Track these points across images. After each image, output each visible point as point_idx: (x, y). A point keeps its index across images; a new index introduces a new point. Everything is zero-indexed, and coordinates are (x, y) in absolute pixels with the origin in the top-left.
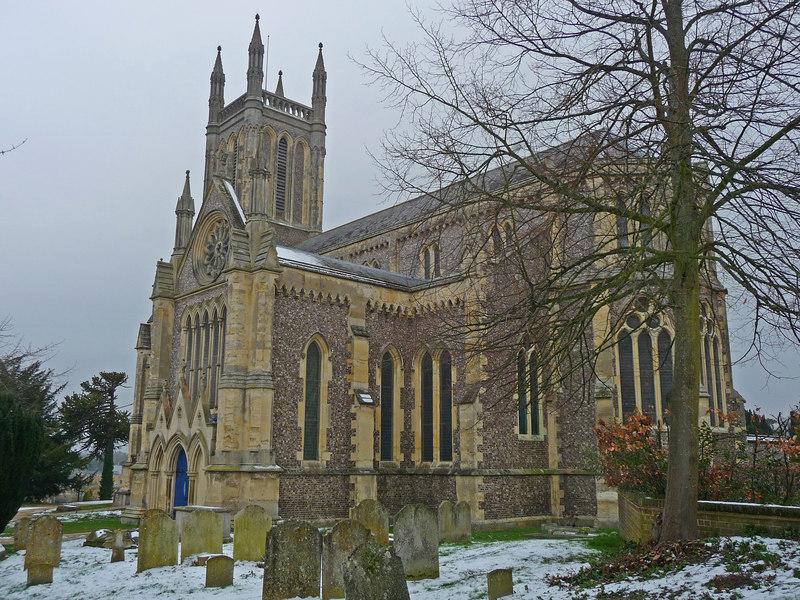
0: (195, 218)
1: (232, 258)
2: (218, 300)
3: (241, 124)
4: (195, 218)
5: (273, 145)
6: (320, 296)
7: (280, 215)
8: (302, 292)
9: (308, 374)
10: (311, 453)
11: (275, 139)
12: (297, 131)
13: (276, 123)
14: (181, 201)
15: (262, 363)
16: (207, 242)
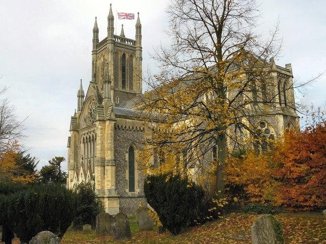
0: (85, 98)
1: (97, 116)
2: (94, 132)
3: (106, 50)
4: (85, 98)
5: (119, 57)
6: (133, 128)
7: (124, 86)
8: (126, 127)
9: (129, 158)
10: (132, 188)
11: (120, 56)
12: (130, 51)
13: (120, 48)
14: (79, 92)
15: (109, 156)
16: (89, 108)
